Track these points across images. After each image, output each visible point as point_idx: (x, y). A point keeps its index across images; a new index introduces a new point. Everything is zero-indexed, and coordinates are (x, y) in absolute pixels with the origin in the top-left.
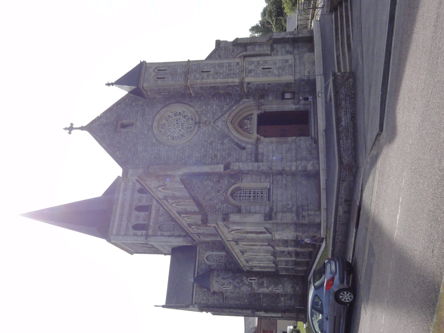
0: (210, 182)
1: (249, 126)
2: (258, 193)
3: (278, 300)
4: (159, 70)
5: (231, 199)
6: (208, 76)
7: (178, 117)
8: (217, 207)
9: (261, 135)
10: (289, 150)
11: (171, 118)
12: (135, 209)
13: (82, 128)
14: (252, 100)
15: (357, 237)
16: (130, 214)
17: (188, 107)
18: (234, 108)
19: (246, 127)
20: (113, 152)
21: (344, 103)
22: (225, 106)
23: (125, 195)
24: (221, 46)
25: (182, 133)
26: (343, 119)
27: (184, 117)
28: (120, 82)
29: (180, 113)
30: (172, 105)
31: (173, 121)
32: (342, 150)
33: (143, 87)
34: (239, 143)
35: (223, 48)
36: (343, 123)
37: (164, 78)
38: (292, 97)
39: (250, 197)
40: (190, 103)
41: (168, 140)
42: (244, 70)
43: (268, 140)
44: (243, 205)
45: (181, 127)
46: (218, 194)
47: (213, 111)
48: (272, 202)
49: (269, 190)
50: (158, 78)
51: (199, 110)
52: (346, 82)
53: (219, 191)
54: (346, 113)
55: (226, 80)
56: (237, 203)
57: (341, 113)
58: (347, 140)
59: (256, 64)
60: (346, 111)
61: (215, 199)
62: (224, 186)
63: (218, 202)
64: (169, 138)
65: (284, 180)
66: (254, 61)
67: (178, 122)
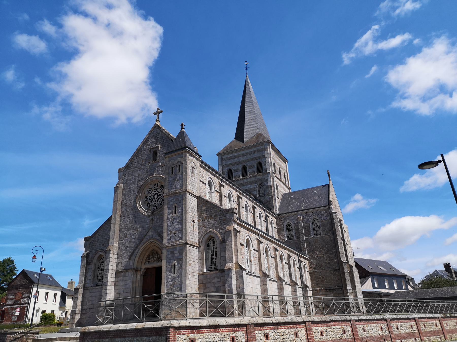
4: (179, 166)
5: (98, 255)
6: (171, 213)
12: (259, 162)
16: (239, 163)
23: (254, 153)
24: (228, 215)
28: (182, 135)
35: (224, 218)
37: (172, 174)
44: (92, 267)
56: (95, 260)
59: (179, 257)
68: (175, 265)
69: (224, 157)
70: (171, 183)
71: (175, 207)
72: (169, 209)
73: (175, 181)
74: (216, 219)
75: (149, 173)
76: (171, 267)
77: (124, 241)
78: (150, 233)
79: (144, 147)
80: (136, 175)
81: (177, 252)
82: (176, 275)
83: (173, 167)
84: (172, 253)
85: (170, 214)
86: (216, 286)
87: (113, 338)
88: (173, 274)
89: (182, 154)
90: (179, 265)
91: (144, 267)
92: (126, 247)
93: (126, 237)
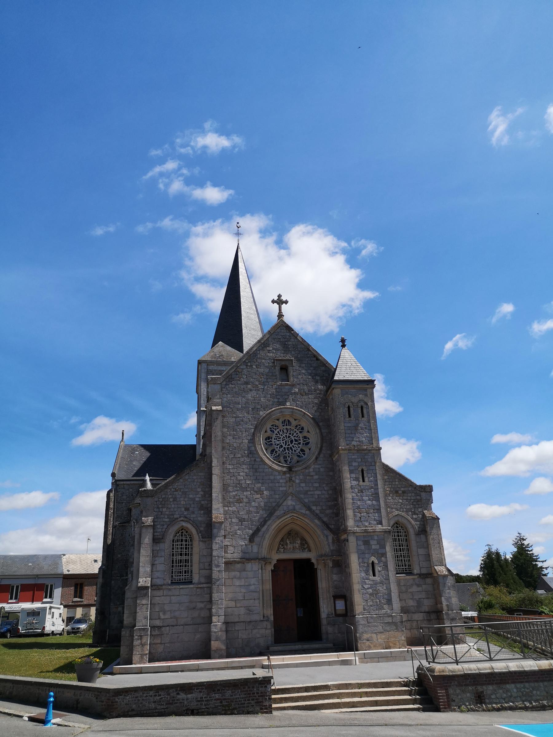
0: (200, 496)
1: (290, 546)
2: (186, 566)
3: (118, 603)
4: (362, 407)
5: (175, 528)
6: (357, 479)
7: (302, 442)
8: (164, 510)
9: (275, 566)
10: (250, 611)
11: (300, 432)
13: (280, 315)
14: (332, 548)
15: (9, 717)
17: (316, 453)
18: (316, 521)
19: (288, 542)
20: (245, 361)
21: (217, 697)
22: (319, 508)
24: (423, 495)
25: (277, 450)
26: (189, 696)
27: (302, 450)
29: (308, 443)
30: (318, 431)
31: (295, 434)
32: (137, 694)
33: (333, 389)
34: (261, 533)
36: (182, 696)
37: (350, 416)
38: (338, 612)
39: (181, 555)
40: (321, 455)
41: (266, 432)
42: (369, 534)
43: (268, 576)
44: (166, 546)
45: (286, 447)
46: (183, 509)
47: (310, 491)
48: (170, 590)
49: (191, 583)
50: (349, 407)
51: (311, 470)
52: (253, 700)
53: (187, 509)
54: (199, 701)
55: (350, 506)
56: (170, 536)
57: (200, 692)
58: (155, 702)
60: (203, 701)
61: (176, 506)
62: (194, 516)
63: (172, 510)
64: (269, 432)
65: (202, 605)
66: (385, 548)
67: (294, 442)
68: (373, 563)
69: (211, 367)
70: (349, 432)
71: (362, 471)
72: (351, 472)
73: (357, 429)
74: (405, 498)
75: (276, 400)
76: (368, 566)
77: (234, 509)
78: (290, 502)
79: (262, 353)
80: (249, 396)
81: (375, 542)
82: (377, 578)
83: (351, 405)
84: (366, 543)
85: (354, 480)
86: (416, 597)
87: (501, 683)
88: (372, 577)
89: (366, 390)
90: (382, 564)
91: (276, 557)
92: (241, 520)
93: (239, 501)
